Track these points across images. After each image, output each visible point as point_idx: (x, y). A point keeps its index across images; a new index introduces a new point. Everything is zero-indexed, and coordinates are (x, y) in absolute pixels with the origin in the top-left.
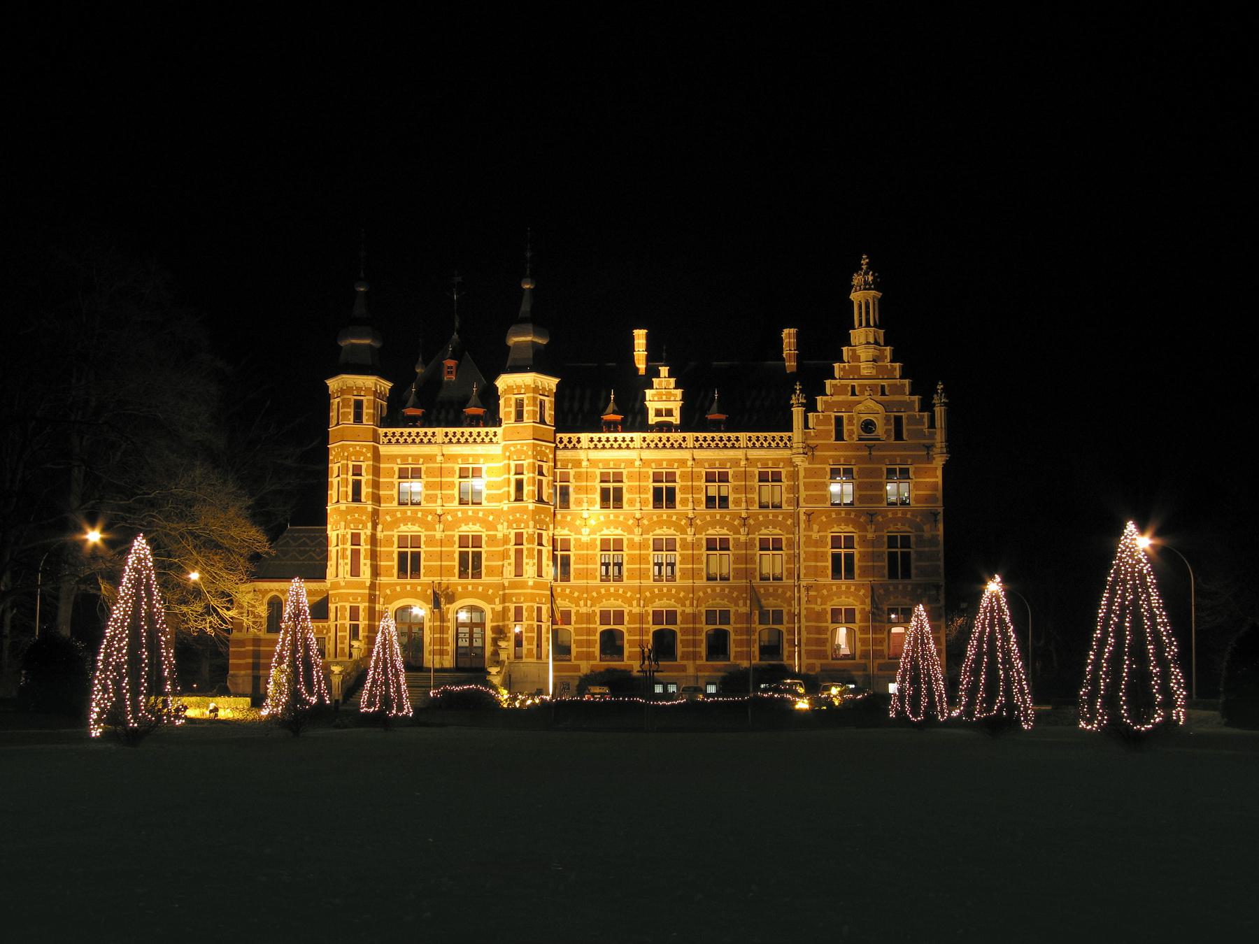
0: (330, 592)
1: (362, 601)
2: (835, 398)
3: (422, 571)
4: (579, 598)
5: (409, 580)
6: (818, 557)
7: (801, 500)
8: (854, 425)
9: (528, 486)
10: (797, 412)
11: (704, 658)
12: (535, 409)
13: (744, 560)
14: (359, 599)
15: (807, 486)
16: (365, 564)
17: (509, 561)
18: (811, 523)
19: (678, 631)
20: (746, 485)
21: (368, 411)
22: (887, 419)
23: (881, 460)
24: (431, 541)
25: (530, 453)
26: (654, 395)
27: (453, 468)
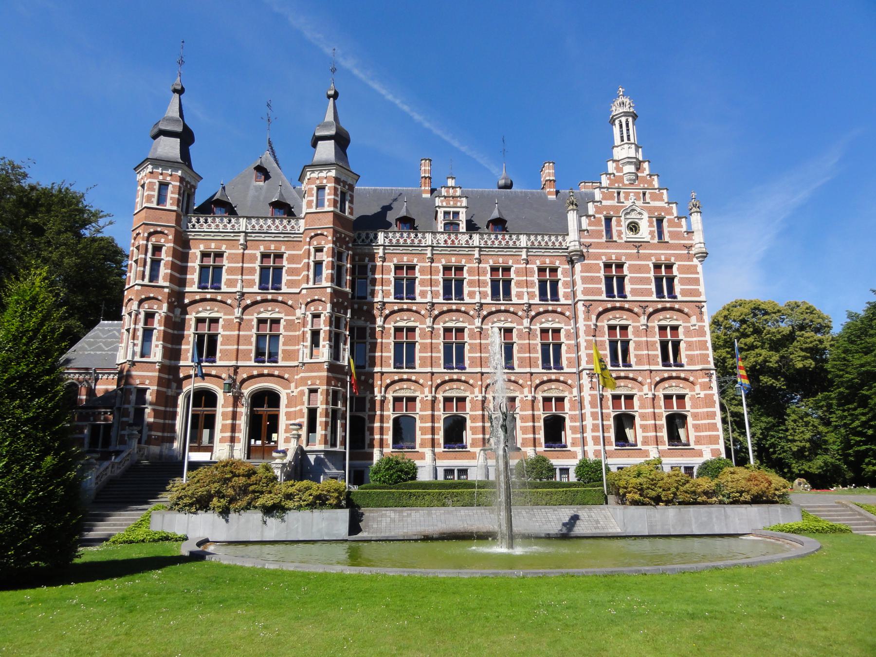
1: (320, 384)
2: (605, 203)
3: (218, 354)
8: (621, 226)
11: (442, 445)
12: (336, 198)
13: (528, 349)
14: (318, 382)
15: (585, 280)
16: (157, 346)
17: (305, 344)
21: (173, 196)
23: (647, 257)
25: (330, 238)
27: (255, 254)
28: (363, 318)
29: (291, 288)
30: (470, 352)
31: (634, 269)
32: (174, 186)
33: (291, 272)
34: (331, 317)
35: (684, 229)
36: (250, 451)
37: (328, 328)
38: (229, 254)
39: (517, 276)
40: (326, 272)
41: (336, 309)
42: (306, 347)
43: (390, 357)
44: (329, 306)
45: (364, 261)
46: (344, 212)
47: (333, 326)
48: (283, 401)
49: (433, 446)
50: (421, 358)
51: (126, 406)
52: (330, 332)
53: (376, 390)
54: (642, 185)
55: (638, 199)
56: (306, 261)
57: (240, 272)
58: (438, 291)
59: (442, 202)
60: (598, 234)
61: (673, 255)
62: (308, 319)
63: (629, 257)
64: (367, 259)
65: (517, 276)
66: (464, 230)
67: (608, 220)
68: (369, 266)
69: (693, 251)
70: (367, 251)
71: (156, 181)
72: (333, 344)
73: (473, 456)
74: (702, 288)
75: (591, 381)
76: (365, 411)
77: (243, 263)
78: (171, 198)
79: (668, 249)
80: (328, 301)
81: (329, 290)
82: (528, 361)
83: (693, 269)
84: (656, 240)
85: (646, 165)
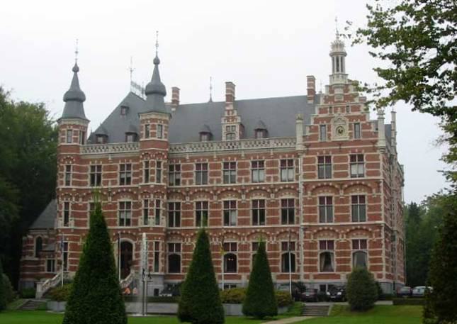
2: (321, 116)
23: (346, 151)
55: (343, 111)
61: (330, 150)
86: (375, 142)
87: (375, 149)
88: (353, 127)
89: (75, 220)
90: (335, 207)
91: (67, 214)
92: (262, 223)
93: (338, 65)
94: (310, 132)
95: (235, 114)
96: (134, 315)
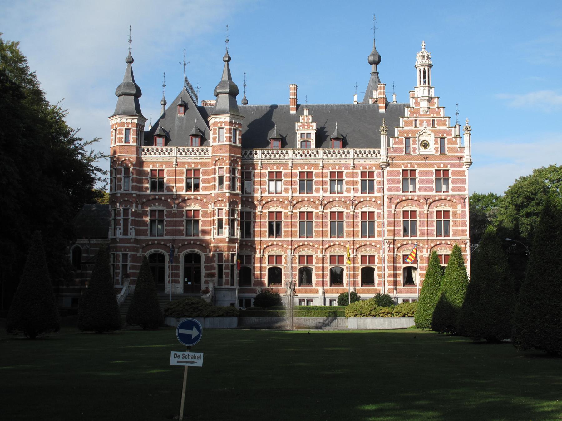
0: (110, 245)
2: (406, 128)
4: (318, 248)
5: (274, 239)
6: (428, 224)
7: (385, 189)
9: (226, 182)
10: (383, 138)
12: (231, 135)
14: (128, 250)
17: (215, 227)
18: (391, 204)
19: (314, 268)
20: (291, 180)
22: (436, 141)
23: (432, 165)
24: (205, 214)
25: (227, 162)
26: (300, 126)
28: (249, 206)
29: (205, 191)
30: (315, 228)
31: (422, 173)
32: (133, 130)
33: (205, 181)
34: (229, 211)
35: (458, 146)
36: (186, 288)
37: (227, 218)
38: (167, 170)
39: (347, 178)
40: (226, 183)
41: (232, 205)
42: (215, 229)
43: (266, 231)
44: (228, 204)
45: (249, 169)
46: (236, 143)
47: (231, 216)
48: (203, 259)
49: (323, 285)
50: (285, 231)
51: (118, 263)
52: (229, 219)
53: (258, 251)
54: (432, 115)
55: (429, 125)
56: (214, 176)
57: (175, 182)
58: (296, 188)
59: (300, 126)
60: (399, 150)
61: (449, 163)
62: (216, 212)
63: (419, 165)
64: (251, 168)
65: (347, 178)
66: (314, 148)
67: (407, 139)
68: (252, 173)
69: (463, 161)
70: (251, 163)
71: (123, 128)
72: (230, 227)
73: (317, 291)
74: (466, 186)
75: (389, 246)
76: (251, 264)
77: (176, 176)
78: (133, 138)
79: (446, 159)
80: (227, 201)
81: (228, 194)
82: (352, 233)
83: (462, 173)
84: (439, 154)
85: (436, 100)
86: (460, 158)
87: (460, 165)
88: (439, 142)
89: (135, 229)
90: (131, 220)
91: (126, 221)
92: (341, 235)
93: (424, 77)
94: (395, 144)
95: (311, 120)
96: (472, 341)
